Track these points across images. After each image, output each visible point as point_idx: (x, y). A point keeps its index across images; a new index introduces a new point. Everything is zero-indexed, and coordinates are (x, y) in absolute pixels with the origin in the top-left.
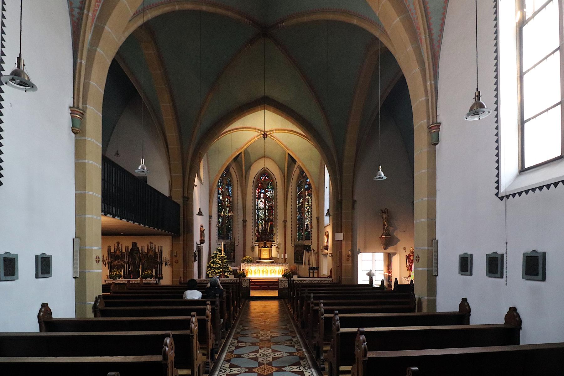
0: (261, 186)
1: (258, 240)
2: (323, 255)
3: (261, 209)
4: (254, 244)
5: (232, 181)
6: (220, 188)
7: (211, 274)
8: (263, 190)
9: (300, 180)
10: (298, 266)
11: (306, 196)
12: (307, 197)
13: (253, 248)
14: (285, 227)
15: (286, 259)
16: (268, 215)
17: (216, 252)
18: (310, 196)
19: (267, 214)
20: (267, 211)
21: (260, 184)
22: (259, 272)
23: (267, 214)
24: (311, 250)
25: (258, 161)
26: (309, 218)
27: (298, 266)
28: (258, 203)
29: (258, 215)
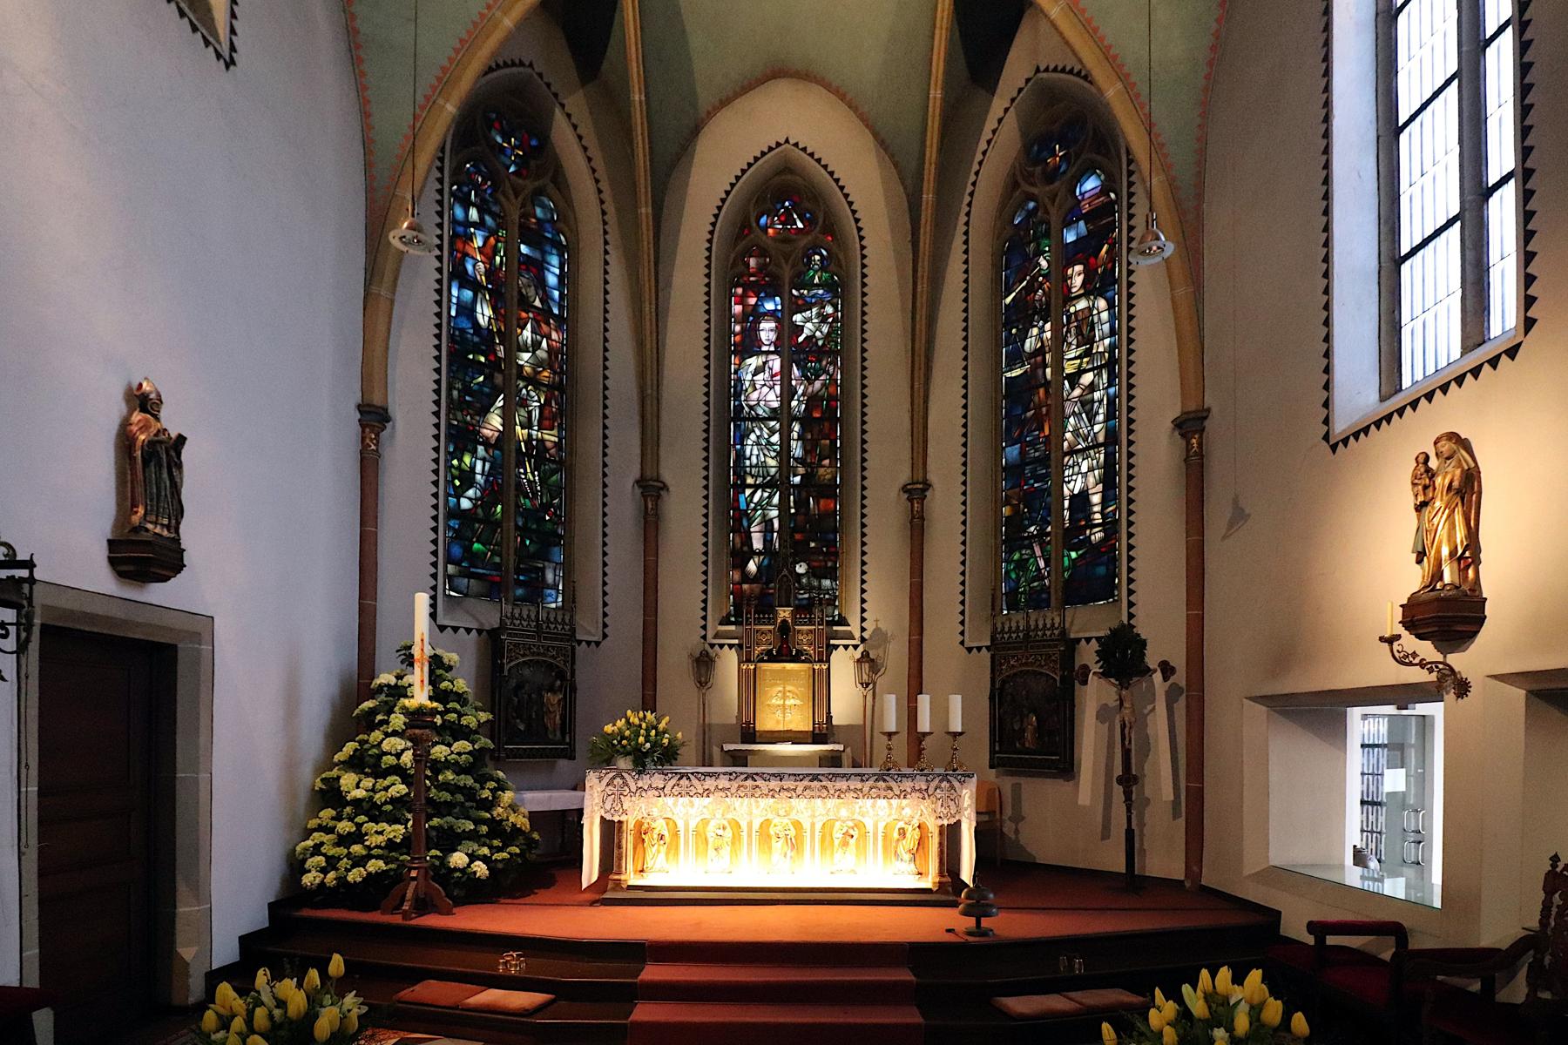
0: (761, 268)
1: (738, 613)
2: (1261, 709)
3: (758, 419)
4: (710, 639)
5: (566, 217)
6: (478, 242)
7: (328, 858)
8: (771, 297)
9: (1021, 205)
10: (1016, 788)
11: (1070, 299)
12: (1082, 304)
13: (704, 664)
14: (917, 528)
15: (925, 734)
16: (806, 451)
17: (393, 681)
18: (1100, 293)
19: (797, 449)
20: (796, 427)
21: (753, 262)
22: (736, 839)
23: (797, 449)
24: (1148, 671)
25: (738, 103)
26: (1097, 446)
27: (1016, 788)
28: (739, 381)
29: (741, 456)
